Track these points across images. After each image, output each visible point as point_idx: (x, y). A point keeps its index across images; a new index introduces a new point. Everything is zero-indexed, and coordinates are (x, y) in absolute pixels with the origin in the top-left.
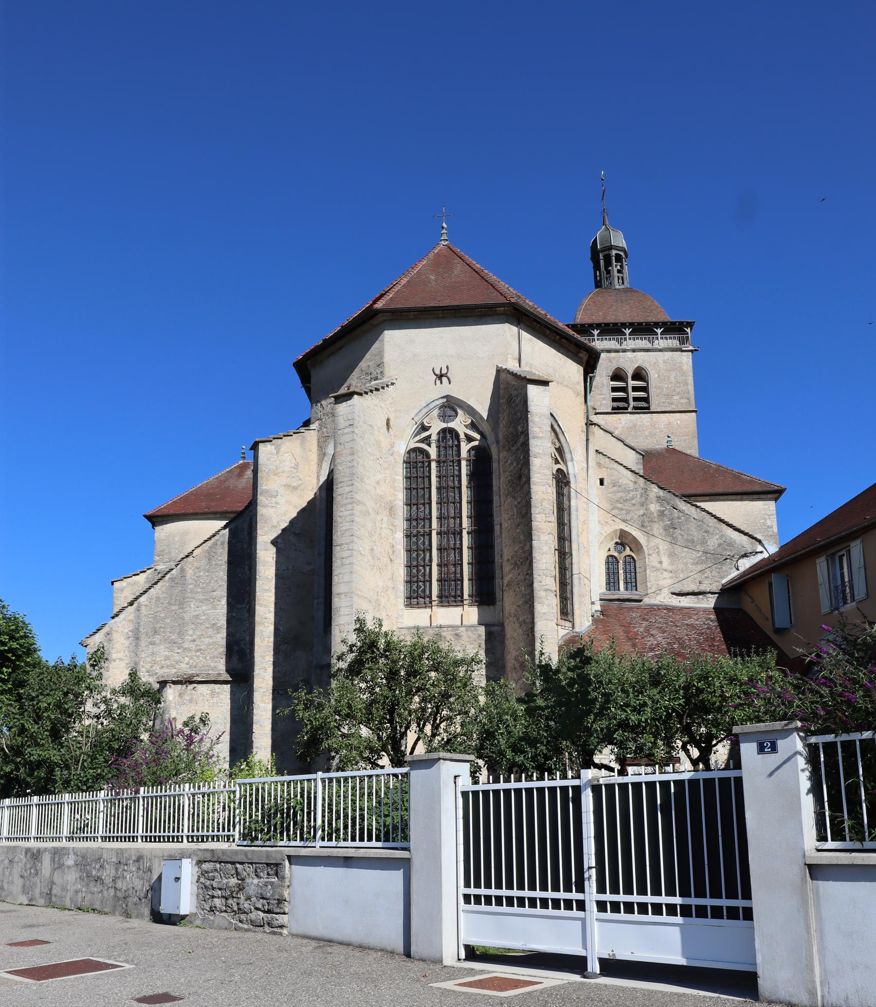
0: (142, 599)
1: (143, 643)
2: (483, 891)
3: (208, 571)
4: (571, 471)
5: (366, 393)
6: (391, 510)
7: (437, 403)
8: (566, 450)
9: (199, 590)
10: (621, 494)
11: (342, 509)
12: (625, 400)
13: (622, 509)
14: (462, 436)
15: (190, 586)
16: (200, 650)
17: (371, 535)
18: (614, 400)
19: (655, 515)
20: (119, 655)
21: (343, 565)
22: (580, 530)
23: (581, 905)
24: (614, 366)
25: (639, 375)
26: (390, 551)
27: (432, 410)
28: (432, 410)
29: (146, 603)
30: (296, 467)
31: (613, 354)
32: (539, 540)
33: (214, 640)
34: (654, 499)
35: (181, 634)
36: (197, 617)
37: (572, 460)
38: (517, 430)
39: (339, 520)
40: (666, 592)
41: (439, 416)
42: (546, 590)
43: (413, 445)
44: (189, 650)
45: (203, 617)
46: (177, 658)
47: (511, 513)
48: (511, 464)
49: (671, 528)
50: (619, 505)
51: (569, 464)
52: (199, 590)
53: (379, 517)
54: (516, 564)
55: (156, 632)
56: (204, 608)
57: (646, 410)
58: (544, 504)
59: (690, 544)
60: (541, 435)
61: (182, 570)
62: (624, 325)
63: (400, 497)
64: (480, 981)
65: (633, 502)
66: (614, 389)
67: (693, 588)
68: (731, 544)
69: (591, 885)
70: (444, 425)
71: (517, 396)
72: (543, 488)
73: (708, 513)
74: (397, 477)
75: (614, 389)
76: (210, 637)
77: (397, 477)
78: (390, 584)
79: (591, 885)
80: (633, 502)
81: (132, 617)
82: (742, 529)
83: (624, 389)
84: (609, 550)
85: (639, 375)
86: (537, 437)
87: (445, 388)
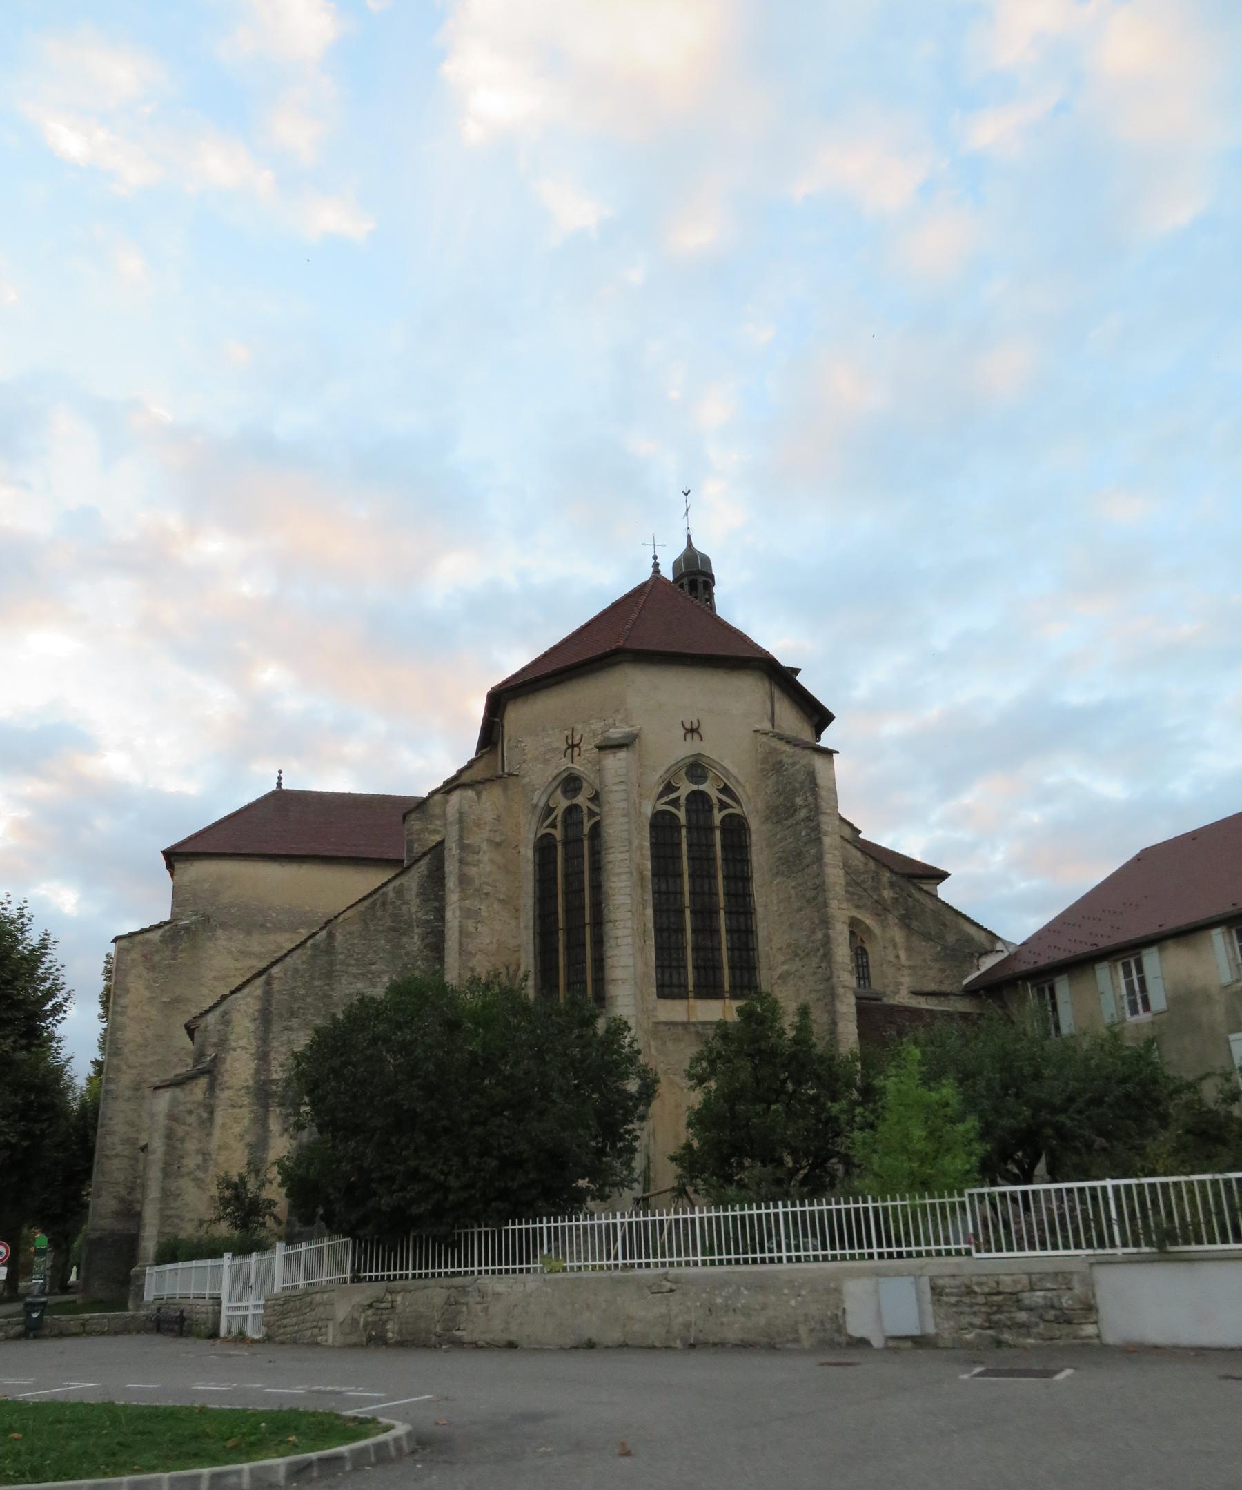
0: (275, 971)
1: (275, 1028)
3: (365, 939)
9: (353, 962)
11: (615, 879)
14: (715, 801)
15: (341, 957)
19: (889, 902)
20: (243, 1043)
29: (281, 975)
30: (498, 819)
34: (887, 885)
39: (610, 892)
40: (904, 991)
42: (845, 987)
49: (906, 921)
52: (353, 962)
55: (293, 1014)
59: (927, 937)
61: (331, 936)
67: (933, 987)
68: (969, 940)
70: (694, 787)
72: (835, 871)
81: (259, 992)
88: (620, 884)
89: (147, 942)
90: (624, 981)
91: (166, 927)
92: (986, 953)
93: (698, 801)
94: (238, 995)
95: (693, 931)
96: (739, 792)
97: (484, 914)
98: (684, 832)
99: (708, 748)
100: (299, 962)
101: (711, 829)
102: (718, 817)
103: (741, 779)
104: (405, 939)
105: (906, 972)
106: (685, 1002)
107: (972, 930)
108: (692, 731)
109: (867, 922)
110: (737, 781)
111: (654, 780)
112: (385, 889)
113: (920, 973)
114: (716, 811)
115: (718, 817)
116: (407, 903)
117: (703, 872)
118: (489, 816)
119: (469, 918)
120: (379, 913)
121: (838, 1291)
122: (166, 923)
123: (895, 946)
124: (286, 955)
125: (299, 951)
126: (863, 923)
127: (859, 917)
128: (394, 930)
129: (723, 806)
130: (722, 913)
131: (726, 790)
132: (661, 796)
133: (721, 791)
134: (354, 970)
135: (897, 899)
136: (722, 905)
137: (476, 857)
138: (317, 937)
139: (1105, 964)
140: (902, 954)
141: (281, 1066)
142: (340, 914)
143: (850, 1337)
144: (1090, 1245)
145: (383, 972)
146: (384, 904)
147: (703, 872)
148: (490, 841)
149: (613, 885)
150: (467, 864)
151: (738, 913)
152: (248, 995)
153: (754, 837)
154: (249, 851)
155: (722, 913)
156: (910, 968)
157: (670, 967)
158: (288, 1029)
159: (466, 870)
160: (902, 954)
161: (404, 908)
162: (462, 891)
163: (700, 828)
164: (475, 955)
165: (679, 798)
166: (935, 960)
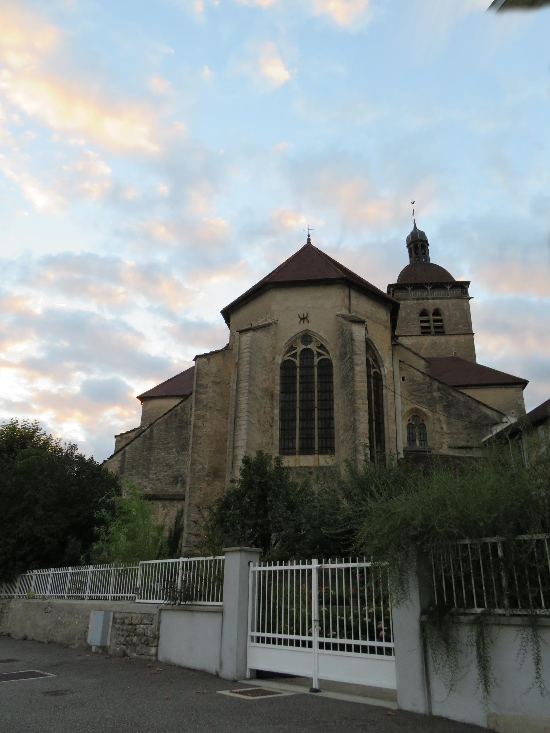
2: (266, 635)
4: (383, 373)
5: (258, 329)
6: (272, 396)
7: (301, 334)
8: (379, 361)
9: (160, 443)
10: (416, 387)
11: (241, 396)
12: (429, 327)
13: (416, 396)
14: (315, 353)
16: (159, 479)
18: (422, 328)
19: (437, 399)
21: (240, 429)
22: (389, 408)
23: (310, 645)
24: (422, 307)
25: (437, 312)
26: (271, 421)
30: (219, 371)
31: (421, 301)
32: (359, 415)
33: (168, 473)
35: (148, 469)
36: (158, 459)
37: (383, 366)
40: (445, 447)
41: (302, 341)
43: (286, 358)
44: (152, 479)
45: (162, 460)
46: (145, 484)
48: (343, 369)
49: (447, 408)
50: (415, 393)
51: (382, 369)
52: (160, 443)
53: (264, 401)
54: (346, 430)
55: (133, 468)
56: (163, 454)
57: (442, 333)
58: (362, 393)
60: (360, 353)
61: (152, 431)
62: (427, 284)
63: (277, 388)
64: (266, 695)
65: (423, 391)
66: (422, 321)
67: (463, 444)
68: (486, 417)
69: (315, 630)
70: (305, 347)
71: (347, 330)
73: (470, 397)
75: (422, 321)
76: (166, 471)
79: (315, 630)
80: (423, 391)
81: (119, 459)
82: (493, 408)
83: (428, 321)
84: (409, 420)
85: (437, 312)
86: (358, 354)
87: (304, 326)
88: (244, 398)
89: (129, 437)
90: (242, 447)
91: (137, 431)
92: (496, 424)
93: (307, 353)
94: (111, 460)
95: (300, 420)
96: (328, 348)
97: (208, 417)
98: (298, 370)
99: (312, 326)
100: (137, 444)
101: (313, 367)
102: (316, 360)
103: (328, 341)
104: (184, 431)
105: (446, 436)
106: (294, 457)
107: (488, 412)
108: (304, 319)
109: (424, 410)
110: (327, 342)
111: (282, 344)
112: (177, 408)
113: (455, 436)
114: (315, 358)
115: (316, 360)
116: (186, 414)
117: (307, 389)
118: (214, 370)
119: (199, 419)
120: (174, 419)
121: (88, 617)
122: (137, 429)
123: (440, 422)
124: (132, 441)
125: (138, 439)
126: (422, 410)
127: (420, 408)
128: (179, 427)
129: (319, 354)
130: (316, 410)
131: (322, 347)
132: (288, 352)
133: (318, 348)
134: (161, 447)
135: (442, 397)
136: (316, 405)
137: (205, 390)
138: (146, 432)
139: (541, 427)
140: (444, 426)
141: (127, 492)
142: (156, 421)
143: (88, 644)
144: (163, 599)
145: (173, 447)
146: (176, 415)
147: (307, 389)
148: (213, 382)
149: (240, 399)
150: (201, 393)
151: (326, 410)
152: (115, 460)
153: (334, 370)
154: (172, 394)
155: (316, 410)
156: (448, 434)
157: (288, 439)
158: (130, 475)
159: (199, 396)
160: (444, 426)
161: (185, 416)
162: (197, 406)
163: (307, 367)
164: (201, 437)
165: (296, 353)
166: (465, 429)
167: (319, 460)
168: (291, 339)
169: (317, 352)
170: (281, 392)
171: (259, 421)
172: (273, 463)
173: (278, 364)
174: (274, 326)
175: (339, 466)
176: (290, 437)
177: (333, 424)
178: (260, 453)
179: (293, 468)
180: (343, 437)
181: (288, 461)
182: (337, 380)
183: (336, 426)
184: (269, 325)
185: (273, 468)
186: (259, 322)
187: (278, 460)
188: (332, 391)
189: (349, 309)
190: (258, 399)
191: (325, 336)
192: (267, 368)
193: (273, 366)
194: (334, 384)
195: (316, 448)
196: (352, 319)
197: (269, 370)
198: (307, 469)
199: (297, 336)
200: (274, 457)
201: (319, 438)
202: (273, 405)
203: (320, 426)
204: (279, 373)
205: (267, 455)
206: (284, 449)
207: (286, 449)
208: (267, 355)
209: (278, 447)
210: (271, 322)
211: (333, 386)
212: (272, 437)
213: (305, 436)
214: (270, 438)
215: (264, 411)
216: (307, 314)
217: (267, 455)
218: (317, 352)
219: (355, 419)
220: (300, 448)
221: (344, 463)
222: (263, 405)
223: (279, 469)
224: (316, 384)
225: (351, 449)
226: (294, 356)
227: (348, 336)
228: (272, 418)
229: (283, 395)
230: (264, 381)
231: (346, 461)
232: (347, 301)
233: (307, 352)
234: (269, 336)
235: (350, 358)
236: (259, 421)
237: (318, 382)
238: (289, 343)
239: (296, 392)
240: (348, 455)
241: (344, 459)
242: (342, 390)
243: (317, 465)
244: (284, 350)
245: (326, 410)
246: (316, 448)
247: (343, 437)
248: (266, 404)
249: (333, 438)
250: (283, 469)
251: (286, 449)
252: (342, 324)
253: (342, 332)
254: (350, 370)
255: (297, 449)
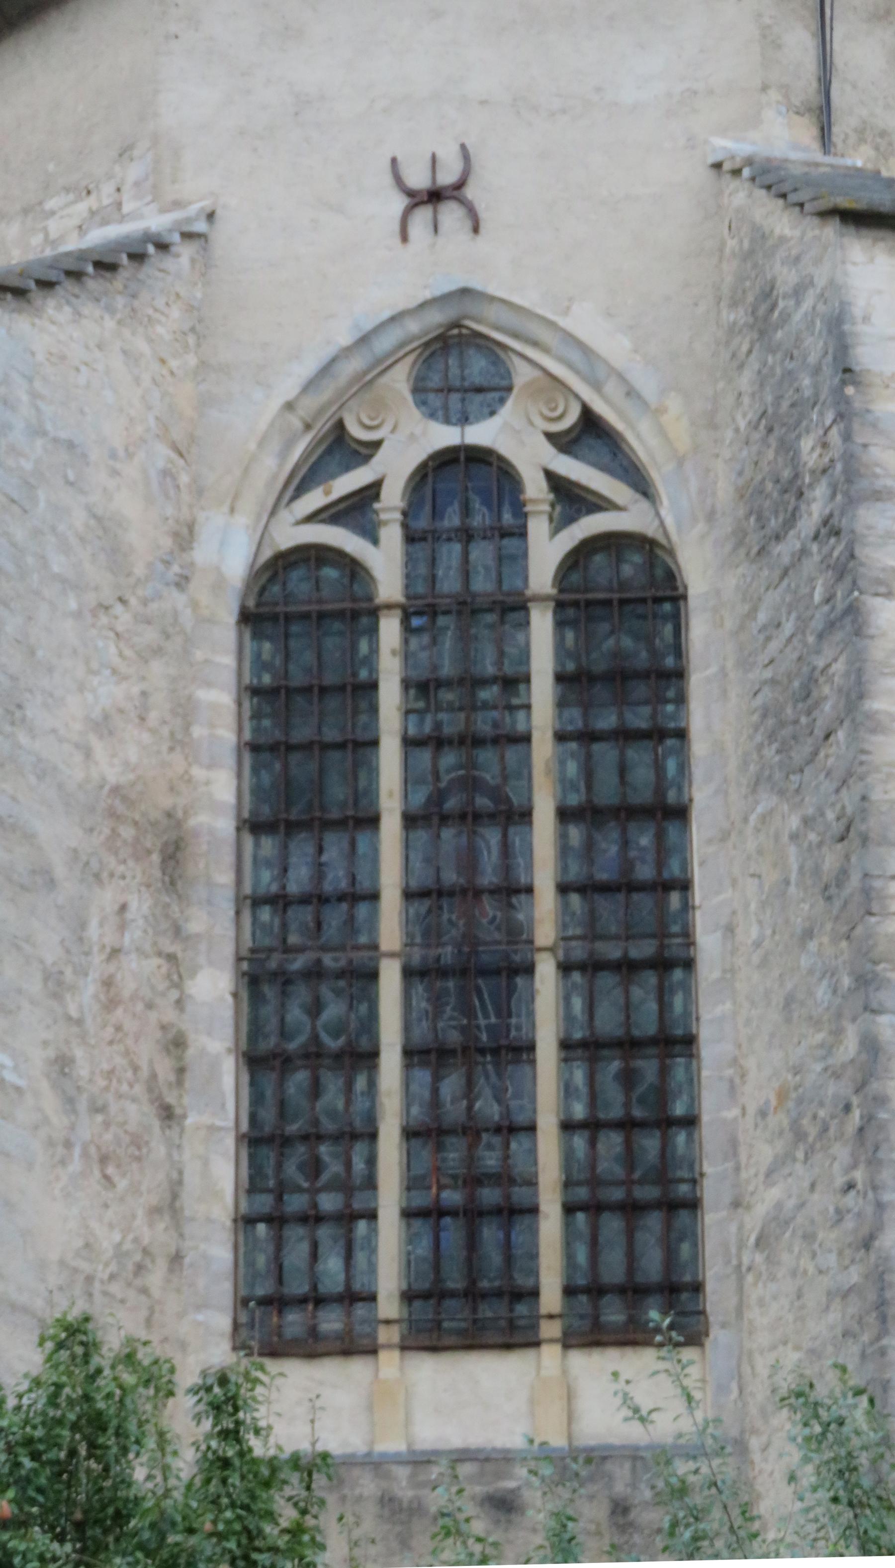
5: (46, 285)
6: (173, 854)
7: (413, 326)
14: (535, 488)
17: (57, 986)
26: (165, 1069)
27: (384, 365)
28: (384, 365)
38: (794, 459)
41: (419, 390)
43: (290, 534)
47: (772, 877)
53: (107, 898)
54: (800, 1136)
63: (217, 794)
70: (446, 436)
71: (798, 292)
74: (204, 695)
77: (204, 695)
78: (158, 1235)
96: (641, 439)
98: (390, 630)
101: (513, 608)
103: (648, 385)
106: (357, 1369)
110: (631, 393)
111: (257, 424)
114: (538, 528)
115: (546, 551)
117: (468, 803)
129: (571, 499)
130: (546, 970)
131: (589, 433)
132: (303, 481)
133: (564, 442)
136: (545, 931)
147: (468, 803)
151: (628, 968)
155: (546, 970)
157: (312, 1218)
163: (464, 612)
165: (373, 491)
167: (570, 1396)
168: (326, 370)
169: (551, 477)
170: (253, 826)
171: (62, 1064)
172: (186, 1427)
173: (219, 584)
174: (185, 255)
175: (741, 1447)
176: (329, 1202)
177: (693, 1081)
178: (73, 1339)
179: (350, 1462)
180: (775, 1193)
181: (309, 1408)
182: (717, 714)
183: (714, 1108)
184: (140, 252)
185: (186, 1463)
186: (54, 227)
187: (225, 1401)
188: (680, 813)
189: (823, 116)
190: (51, 883)
191: (613, 346)
192: (123, 618)
193: (179, 599)
194: (699, 747)
195: (551, 1297)
196: (844, 202)
197: (150, 635)
198: (466, 1469)
199: (385, 343)
200: (188, 1376)
201: (569, 1209)
202: (177, 931)
203: (579, 1111)
204: (228, 660)
205: (129, 1359)
206: (277, 1302)
207: (292, 1314)
208: (128, 504)
209: (224, 1292)
210: (156, 222)
211: (684, 767)
212: (171, 1206)
213: (452, 1197)
214: (154, 1211)
215: (108, 983)
216: (465, 153)
217: (129, 1359)
218: (551, 477)
219: (871, 1046)
220: (408, 1297)
221: (784, 1423)
222: (93, 931)
223: (237, 1472)
224: (543, 748)
225: (846, 1295)
226: (357, 509)
227: (815, 347)
228: (176, 1043)
229: (269, 845)
230: (103, 726)
231: (801, 1398)
232: (800, 43)
233: (464, 480)
234: (141, 345)
235: (829, 528)
236: (62, 1064)
237: (560, 737)
238: (309, 404)
239: (373, 821)
240: (814, 1354)
241: (786, 1382)
242: (767, 801)
243: (558, 1441)
244: (273, 468)
245: (628, 968)
246: (551, 1297)
247: (775, 1193)
248: (122, 927)
249: (694, 1205)
250: (268, 1476)
251: (292, 1314)
252: (760, 244)
253: (763, 311)
254: (831, 625)
255: (388, 1305)
